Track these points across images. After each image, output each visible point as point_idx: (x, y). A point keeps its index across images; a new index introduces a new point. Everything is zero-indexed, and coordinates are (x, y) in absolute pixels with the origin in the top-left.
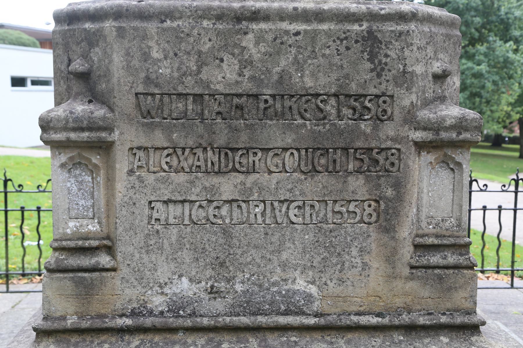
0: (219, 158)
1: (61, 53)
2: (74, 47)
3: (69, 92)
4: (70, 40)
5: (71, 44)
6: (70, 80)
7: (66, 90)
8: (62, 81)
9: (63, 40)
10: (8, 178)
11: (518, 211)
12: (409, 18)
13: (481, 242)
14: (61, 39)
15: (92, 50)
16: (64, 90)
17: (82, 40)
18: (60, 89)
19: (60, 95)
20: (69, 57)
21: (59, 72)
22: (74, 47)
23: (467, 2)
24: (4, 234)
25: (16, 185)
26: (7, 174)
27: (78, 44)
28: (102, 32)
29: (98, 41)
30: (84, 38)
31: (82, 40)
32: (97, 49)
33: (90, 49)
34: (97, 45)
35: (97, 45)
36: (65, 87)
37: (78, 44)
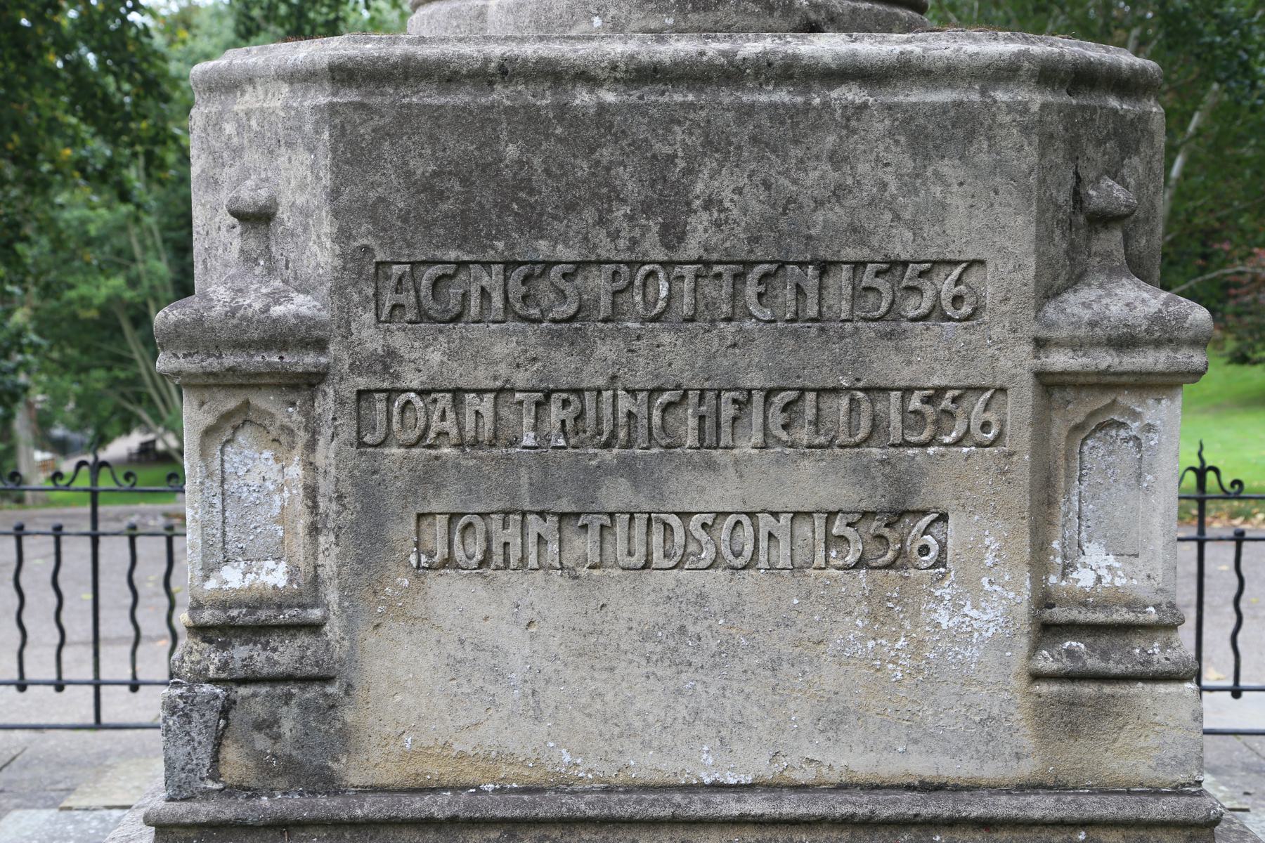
0: (614, 405)
1: (1059, 161)
2: (1090, 151)
3: (1072, 259)
4: (1082, 131)
5: (1084, 140)
6: (1077, 230)
7: (1067, 252)
8: (1058, 232)
9: (1066, 130)
10: (1208, 464)
11: (102, 539)
12: (359, 25)
13: (1244, 573)
14: (1061, 128)
15: (1126, 161)
16: (1061, 253)
17: (1108, 137)
18: (1053, 251)
19: (1051, 265)
20: (1076, 173)
21: (1052, 208)
22: (1090, 151)
23: (480, 3)
24: (90, 637)
25: (1227, 481)
26: (1205, 455)
27: (1100, 143)
28: (1146, 122)
29: (1138, 142)
30: (1111, 131)
31: (1108, 137)
32: (1135, 160)
33: (1123, 159)
34: (1137, 152)
35: (1137, 152)
36: (1064, 245)
37: (1100, 143)
